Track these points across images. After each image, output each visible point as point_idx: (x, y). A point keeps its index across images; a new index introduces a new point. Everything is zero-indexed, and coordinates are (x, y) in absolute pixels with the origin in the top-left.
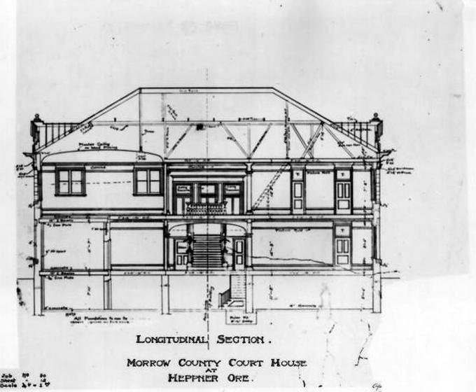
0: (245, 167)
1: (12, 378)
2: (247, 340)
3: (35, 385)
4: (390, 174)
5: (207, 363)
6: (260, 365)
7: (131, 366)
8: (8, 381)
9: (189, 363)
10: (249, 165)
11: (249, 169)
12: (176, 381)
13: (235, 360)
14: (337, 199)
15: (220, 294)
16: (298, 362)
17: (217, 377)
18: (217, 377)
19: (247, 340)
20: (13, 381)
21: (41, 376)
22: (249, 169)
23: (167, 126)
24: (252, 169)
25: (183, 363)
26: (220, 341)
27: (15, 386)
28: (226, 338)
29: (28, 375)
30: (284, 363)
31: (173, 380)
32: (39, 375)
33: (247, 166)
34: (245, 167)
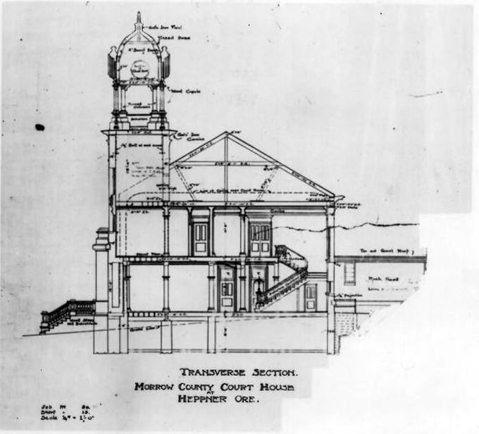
0: (239, 211)
1: (52, 410)
2: (278, 373)
3: (74, 418)
4: (134, 214)
5: (203, 387)
6: (250, 390)
7: (139, 389)
8: (49, 413)
9: (231, 388)
10: (243, 208)
11: (243, 213)
12: (185, 401)
13: (227, 385)
14: (195, 242)
15: (44, 314)
16: (285, 386)
17: (226, 398)
18: (226, 398)
19: (278, 373)
20: (54, 412)
21: (83, 407)
22: (243, 213)
23: (151, 106)
24: (245, 213)
25: (225, 387)
26: (256, 373)
27: (56, 418)
28: (261, 371)
29: (64, 407)
30: (273, 388)
31: (182, 400)
32: (81, 407)
33: (241, 210)
34: (239, 211)
